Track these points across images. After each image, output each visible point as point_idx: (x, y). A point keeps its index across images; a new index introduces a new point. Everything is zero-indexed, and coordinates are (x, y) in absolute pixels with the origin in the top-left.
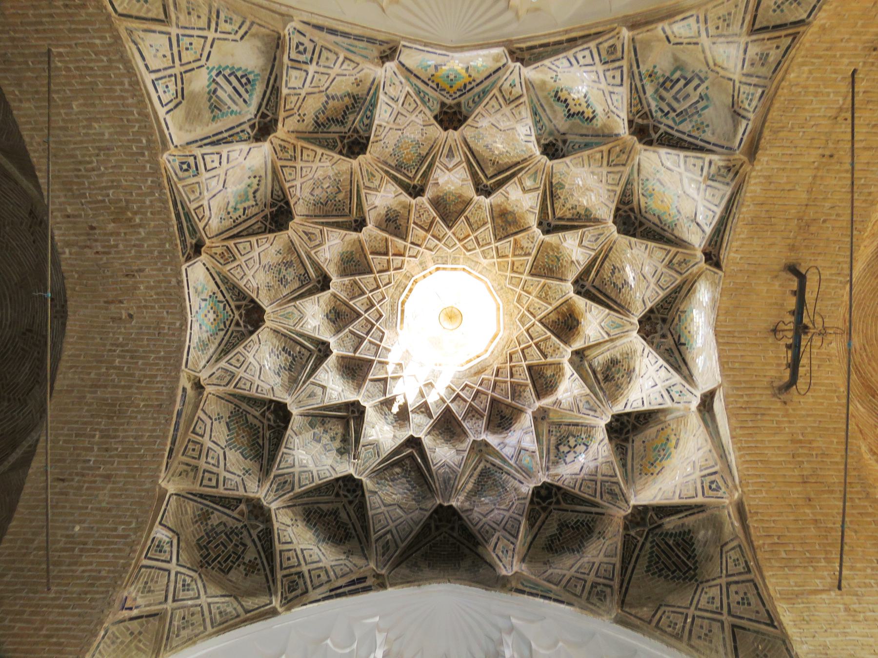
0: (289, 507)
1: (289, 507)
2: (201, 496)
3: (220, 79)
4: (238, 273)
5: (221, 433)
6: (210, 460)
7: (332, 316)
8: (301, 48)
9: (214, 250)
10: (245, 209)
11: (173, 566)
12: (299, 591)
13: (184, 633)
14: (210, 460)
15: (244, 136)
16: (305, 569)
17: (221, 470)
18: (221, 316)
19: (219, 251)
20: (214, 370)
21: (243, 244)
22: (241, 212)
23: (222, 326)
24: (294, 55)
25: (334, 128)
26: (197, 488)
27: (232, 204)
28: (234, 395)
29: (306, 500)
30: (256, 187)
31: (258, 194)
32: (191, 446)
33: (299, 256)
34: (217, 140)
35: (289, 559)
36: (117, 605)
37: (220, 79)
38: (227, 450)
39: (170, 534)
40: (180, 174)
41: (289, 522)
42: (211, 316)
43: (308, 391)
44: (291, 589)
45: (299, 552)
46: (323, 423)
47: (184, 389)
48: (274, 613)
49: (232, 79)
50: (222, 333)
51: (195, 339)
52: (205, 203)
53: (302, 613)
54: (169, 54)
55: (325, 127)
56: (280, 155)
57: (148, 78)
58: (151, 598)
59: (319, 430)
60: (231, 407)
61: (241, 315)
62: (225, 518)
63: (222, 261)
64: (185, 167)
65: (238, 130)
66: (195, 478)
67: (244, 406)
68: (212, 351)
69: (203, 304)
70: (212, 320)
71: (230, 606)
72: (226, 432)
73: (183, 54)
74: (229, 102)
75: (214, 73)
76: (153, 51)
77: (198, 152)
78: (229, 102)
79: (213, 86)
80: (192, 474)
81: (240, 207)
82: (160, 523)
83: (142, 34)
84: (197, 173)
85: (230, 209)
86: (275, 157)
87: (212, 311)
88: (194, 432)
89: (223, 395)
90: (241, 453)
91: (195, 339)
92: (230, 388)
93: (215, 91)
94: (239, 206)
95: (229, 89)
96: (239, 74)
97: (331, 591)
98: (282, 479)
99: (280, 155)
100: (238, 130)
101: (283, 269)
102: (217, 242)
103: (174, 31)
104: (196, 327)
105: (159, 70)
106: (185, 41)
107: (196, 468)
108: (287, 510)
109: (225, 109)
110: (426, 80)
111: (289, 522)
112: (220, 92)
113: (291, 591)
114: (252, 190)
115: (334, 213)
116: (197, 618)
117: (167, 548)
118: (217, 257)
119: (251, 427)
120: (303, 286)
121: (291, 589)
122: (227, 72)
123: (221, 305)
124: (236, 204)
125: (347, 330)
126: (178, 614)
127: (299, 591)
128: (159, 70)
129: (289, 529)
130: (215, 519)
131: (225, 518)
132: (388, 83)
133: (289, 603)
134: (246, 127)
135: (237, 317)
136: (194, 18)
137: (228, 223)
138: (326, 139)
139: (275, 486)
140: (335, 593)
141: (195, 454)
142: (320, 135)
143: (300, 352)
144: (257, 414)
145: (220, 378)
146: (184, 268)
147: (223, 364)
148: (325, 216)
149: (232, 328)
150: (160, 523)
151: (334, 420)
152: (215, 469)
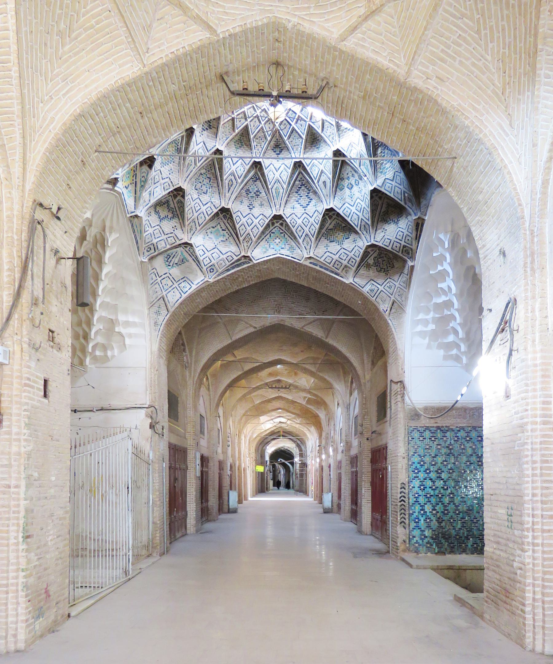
0: (376, 231)
1: (376, 231)
2: (358, 267)
3: (171, 264)
4: (255, 231)
5: (334, 247)
6: (344, 258)
7: (278, 151)
8: (149, 250)
9: (246, 247)
10: (223, 230)
11: (381, 288)
12: (410, 252)
13: (403, 299)
14: (344, 258)
15: (191, 250)
16: (403, 243)
17: (351, 255)
18: (278, 235)
19: (245, 244)
20: (303, 247)
21: (241, 230)
22: (225, 232)
23: (283, 235)
24: (153, 251)
25: (172, 206)
26: (354, 269)
27: (222, 238)
28: (317, 238)
29: (376, 220)
30: (211, 229)
31: (214, 226)
32: (336, 266)
33: (242, 189)
34: (196, 260)
35: (396, 247)
36: (383, 313)
37: (171, 264)
38: (343, 246)
39: (369, 283)
40: (215, 271)
41: (383, 234)
42: (277, 241)
43: (322, 186)
44: (408, 253)
45: (396, 240)
46: (342, 179)
47: (310, 263)
48: (413, 267)
49: (169, 260)
50: (286, 236)
51: (288, 253)
52: (225, 256)
53: (419, 255)
54: (172, 291)
55: (173, 211)
56: (194, 229)
57: (184, 296)
58: (387, 302)
59: (346, 183)
60: (323, 239)
61: (277, 222)
62: (372, 257)
63: (250, 242)
64: (212, 270)
65: (189, 252)
66: (350, 268)
67: (323, 231)
68: (294, 244)
69: (272, 246)
70: (279, 241)
71: (404, 277)
72: (334, 244)
73: (170, 285)
74: (178, 257)
75: (170, 267)
76: (174, 297)
77: (205, 268)
78: (178, 257)
79: (175, 265)
80: (348, 269)
81: (222, 232)
82: (363, 288)
83: (171, 303)
84: (214, 265)
85: (225, 239)
86: (196, 232)
87: (275, 240)
88: (330, 263)
89: (316, 244)
90: (346, 239)
91: (288, 253)
92: (313, 239)
93: (176, 264)
94: (222, 234)
95: (173, 260)
96: (166, 259)
97: (416, 239)
98: (362, 227)
99: (194, 229)
100: (189, 252)
101: (251, 195)
102: (242, 248)
103: (164, 293)
104: (282, 251)
105: (180, 293)
106: (166, 287)
107: (346, 266)
108: (377, 232)
109: (182, 257)
110: (134, 185)
111: (383, 234)
112: (176, 262)
113: (409, 254)
114: (213, 229)
115: (213, 171)
116: (402, 292)
117: (373, 287)
118: (249, 244)
119: (335, 227)
120: (259, 178)
121: (408, 253)
122: (167, 263)
123: (272, 235)
124: (221, 235)
125: (287, 142)
126: (397, 296)
127: (410, 252)
128: (180, 293)
129: (386, 237)
130: (371, 261)
131: (372, 257)
132: (145, 204)
133: (413, 258)
134: (187, 249)
135: (278, 224)
136: (157, 290)
137: (231, 239)
138: (179, 208)
139: (365, 232)
140: (418, 238)
141: (340, 264)
142: (178, 212)
143: (300, 181)
144: (329, 222)
145: (308, 244)
146: (255, 262)
147: (301, 241)
148: (217, 179)
149: (283, 228)
150: (363, 288)
151: (343, 170)
152: (349, 258)
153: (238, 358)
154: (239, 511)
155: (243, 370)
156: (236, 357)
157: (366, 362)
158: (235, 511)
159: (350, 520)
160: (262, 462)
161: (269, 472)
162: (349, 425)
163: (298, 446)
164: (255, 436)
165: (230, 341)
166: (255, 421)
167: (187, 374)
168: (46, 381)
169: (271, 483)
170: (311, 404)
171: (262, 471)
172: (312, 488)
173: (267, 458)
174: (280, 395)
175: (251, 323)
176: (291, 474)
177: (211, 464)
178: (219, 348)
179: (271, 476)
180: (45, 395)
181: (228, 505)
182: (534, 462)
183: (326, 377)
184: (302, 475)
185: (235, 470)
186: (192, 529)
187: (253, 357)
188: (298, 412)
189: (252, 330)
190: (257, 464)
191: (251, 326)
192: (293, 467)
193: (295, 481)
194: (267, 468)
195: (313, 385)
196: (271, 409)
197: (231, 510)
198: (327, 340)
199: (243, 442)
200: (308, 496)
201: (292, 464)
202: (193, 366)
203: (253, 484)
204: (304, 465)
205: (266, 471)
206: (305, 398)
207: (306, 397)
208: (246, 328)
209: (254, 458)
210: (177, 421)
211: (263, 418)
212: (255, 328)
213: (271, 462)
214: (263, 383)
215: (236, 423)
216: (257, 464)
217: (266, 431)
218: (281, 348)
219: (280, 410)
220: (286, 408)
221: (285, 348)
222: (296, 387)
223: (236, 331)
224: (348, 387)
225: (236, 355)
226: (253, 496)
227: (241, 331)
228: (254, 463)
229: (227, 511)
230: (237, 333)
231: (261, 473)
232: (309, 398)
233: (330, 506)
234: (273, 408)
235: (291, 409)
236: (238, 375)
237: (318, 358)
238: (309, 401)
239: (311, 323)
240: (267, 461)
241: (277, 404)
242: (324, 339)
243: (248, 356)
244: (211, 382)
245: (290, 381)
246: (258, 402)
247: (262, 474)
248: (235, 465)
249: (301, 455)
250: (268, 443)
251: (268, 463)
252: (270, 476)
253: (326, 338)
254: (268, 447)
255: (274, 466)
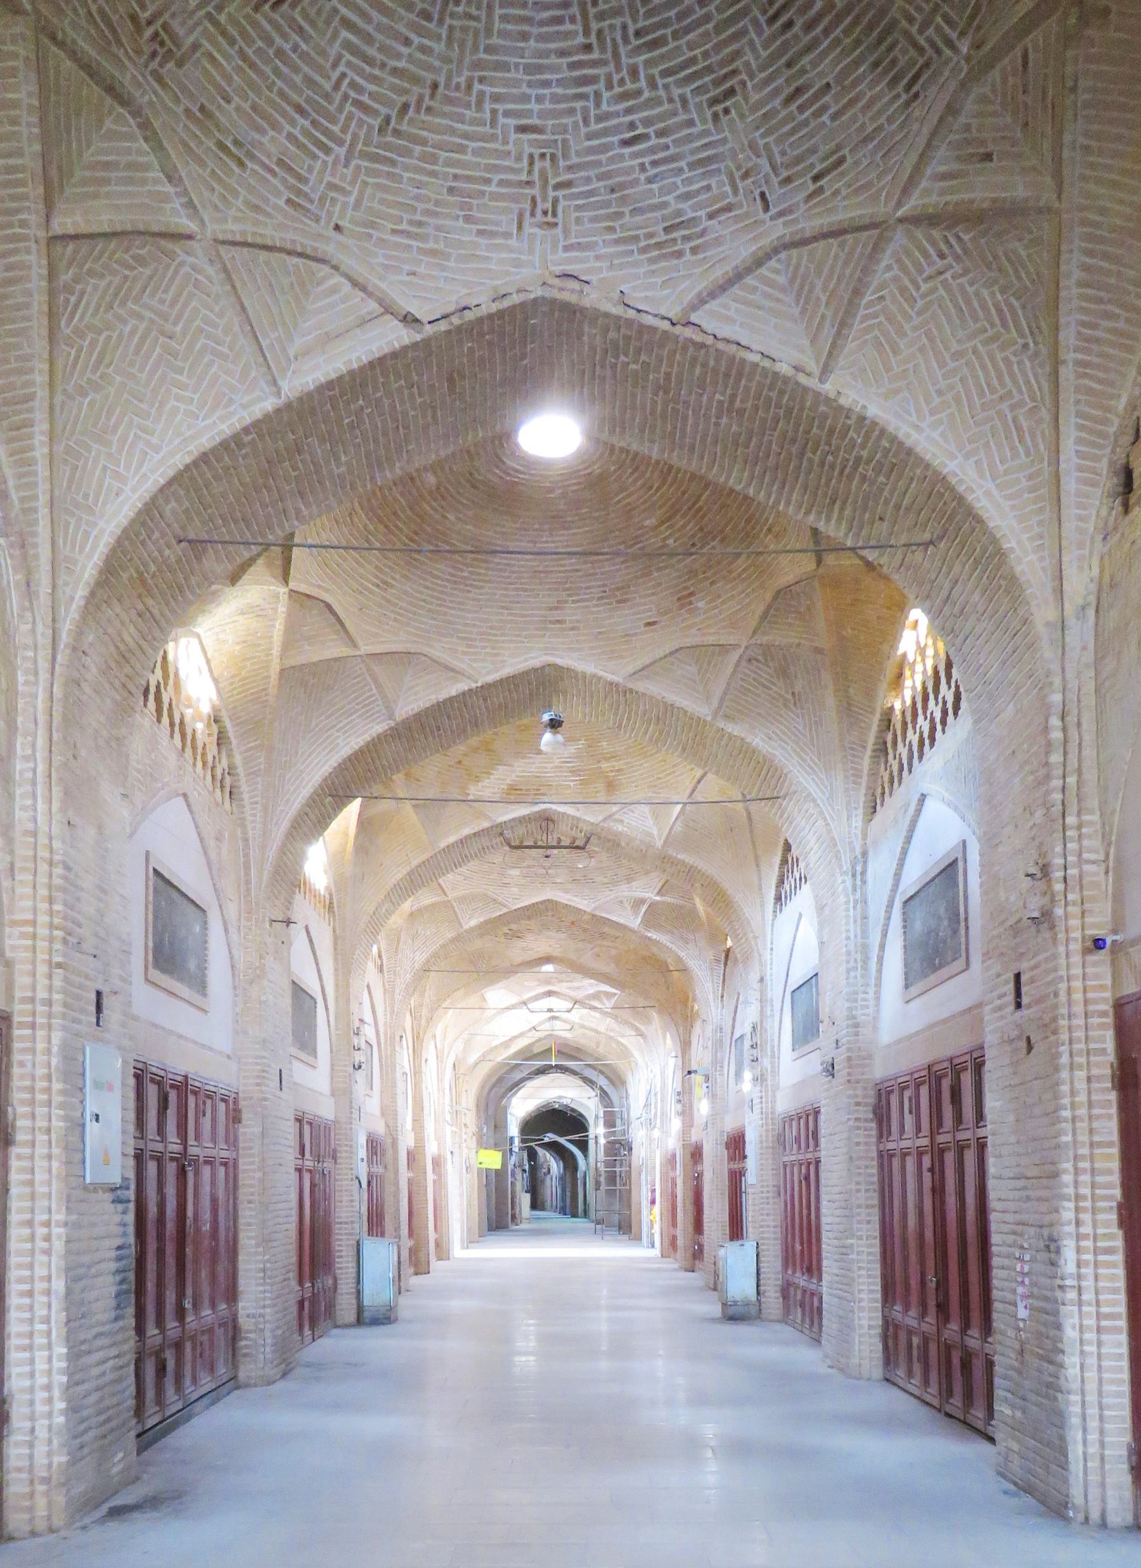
153: (365, 649)
154: (403, 1312)
155: (391, 717)
156: (355, 646)
157: (1070, 485)
158: (384, 1318)
161: (518, 1171)
162: (865, 948)
163: (604, 1095)
164: (472, 1059)
165: (269, 404)
166: (473, 1000)
168: (99, 994)
169: (525, 1199)
170: (658, 927)
171: (498, 1166)
173: (514, 1130)
174: (548, 894)
176: (580, 1175)
178: (206, 441)
180: (98, 1024)
181: (359, 1294)
183: (757, 741)
184: (612, 1178)
185: (396, 1159)
186: (41, 1502)
188: (609, 968)
189: (395, 336)
190: (482, 1144)
191: (388, 309)
192: (586, 1156)
193: (595, 1198)
195: (678, 828)
196: (520, 959)
197: (366, 1314)
198: (828, 388)
200: (639, 1238)
201: (583, 1145)
203: (469, 1205)
204: (619, 1148)
205: (510, 1167)
207: (642, 901)
208: (363, 323)
209: (473, 1128)
210: (205, 995)
211: (497, 995)
212: (409, 320)
213: (523, 1141)
214: (486, 824)
215: (398, 997)
216: (482, 1144)
218: (556, 615)
219: (549, 968)
220: (572, 956)
222: (613, 844)
223: (299, 342)
224: (857, 774)
226: (470, 1242)
227: (328, 339)
229: (351, 1317)
230: (306, 352)
231: (497, 1172)
236: (367, 737)
237: (724, 649)
238: (654, 915)
239: (738, 277)
240: (512, 1138)
241: (539, 944)
242: (812, 383)
245: (591, 816)
246: (473, 923)
247: (500, 1174)
248: (395, 1143)
249: (610, 1122)
250: (517, 1085)
251: (517, 1141)
252: (521, 1182)
253: (826, 371)
255: (532, 1155)
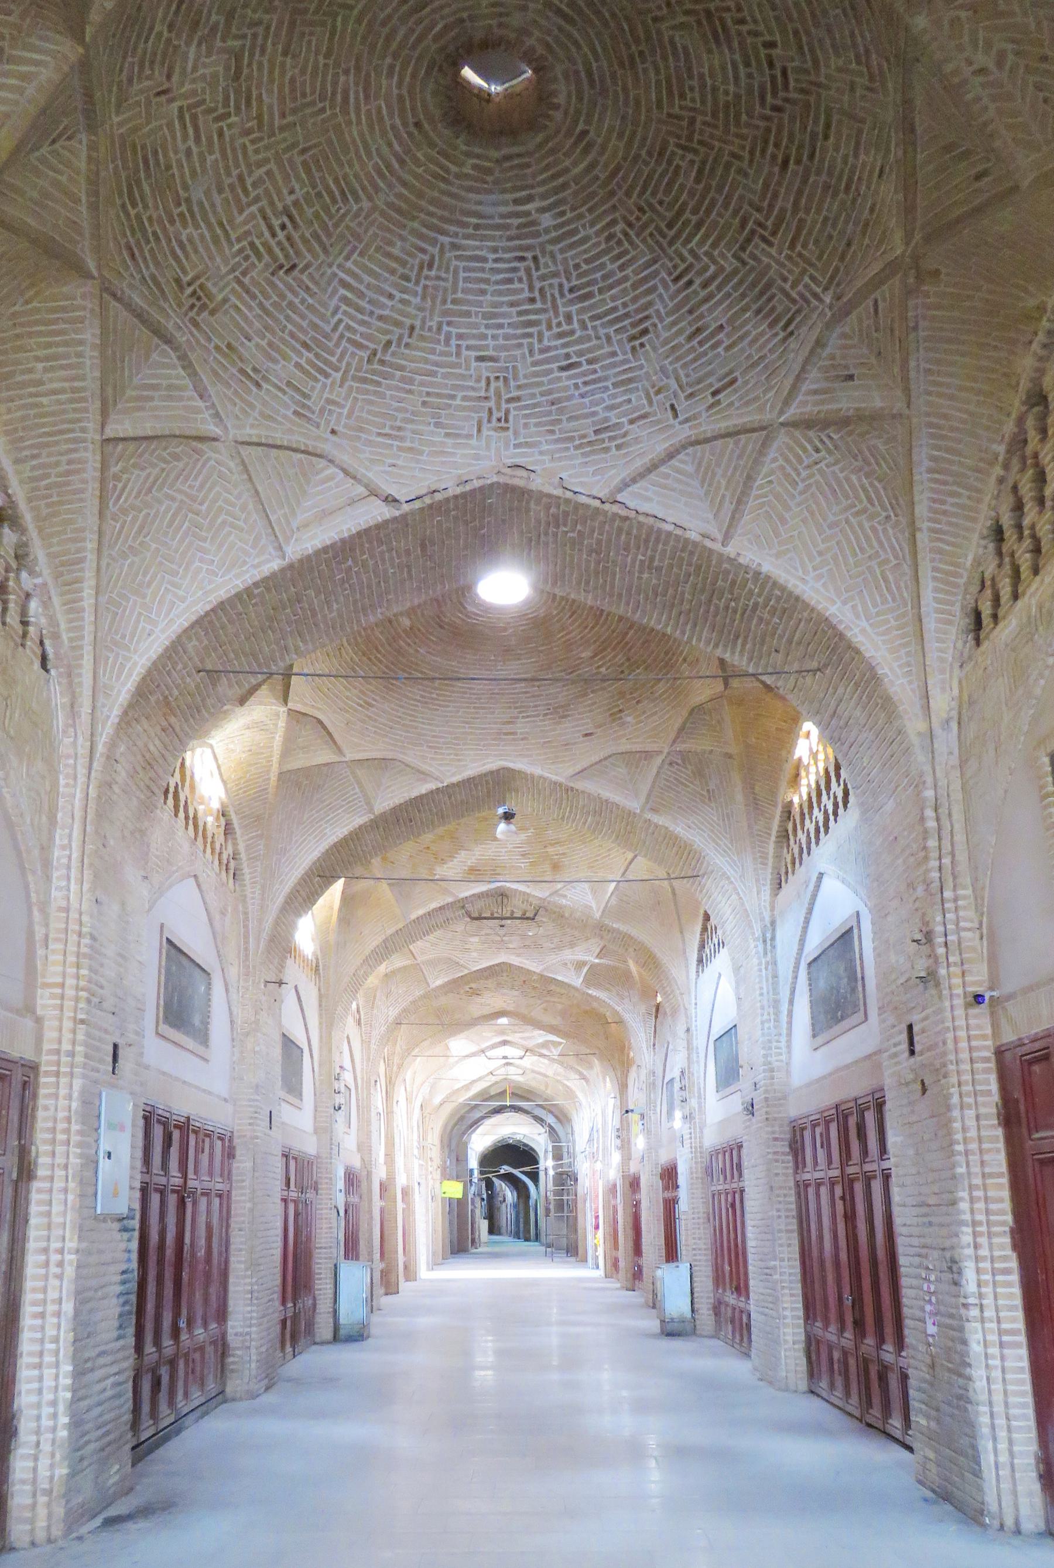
153: (350, 756)
154: (374, 1331)
156: (339, 751)
157: (931, 624)
158: (358, 1336)
159: (803, 1385)
160: (459, 1172)
161: (478, 1200)
164: (437, 1100)
167: (59, 699)
170: (598, 986)
171: (460, 1195)
172: (596, 1241)
173: (473, 1163)
175: (375, 475)
176: (532, 1202)
177: (242, 1164)
178: (223, 593)
179: (485, 1210)
181: (335, 1313)
182: (61, 1251)
183: (679, 830)
187: (408, 759)
188: (556, 1021)
189: (377, 512)
190: (446, 1176)
191: (374, 493)
194: (473, 1190)
195: (614, 901)
197: (342, 1332)
198: (730, 550)
199: (400, 1110)
200: (585, 1260)
201: (534, 1176)
202: (87, 662)
203: (435, 1231)
204: (566, 1179)
205: (470, 1196)
206: (580, 965)
207: (584, 963)
209: (438, 1161)
210: (207, 1046)
211: (459, 1044)
212: (390, 500)
213: (482, 1173)
214: (450, 900)
215: (373, 1046)
216: (446, 1176)
217: (467, 1087)
218: (508, 728)
219: (503, 1021)
221: (521, 727)
224: (764, 857)
225: (344, 747)
226: (434, 1265)
227: (325, 514)
228: (438, 1175)
232: (593, 966)
233: (688, 1313)
234: (487, 1011)
235: (537, 1013)
237: (647, 755)
239: (653, 467)
240: (472, 1170)
241: (493, 1000)
242: (717, 547)
243: (389, 755)
244: (248, 848)
245: (539, 892)
246: (439, 982)
247: (461, 1203)
249: (558, 1156)
251: (476, 1173)
254: (474, 1137)
255: (489, 1185)
